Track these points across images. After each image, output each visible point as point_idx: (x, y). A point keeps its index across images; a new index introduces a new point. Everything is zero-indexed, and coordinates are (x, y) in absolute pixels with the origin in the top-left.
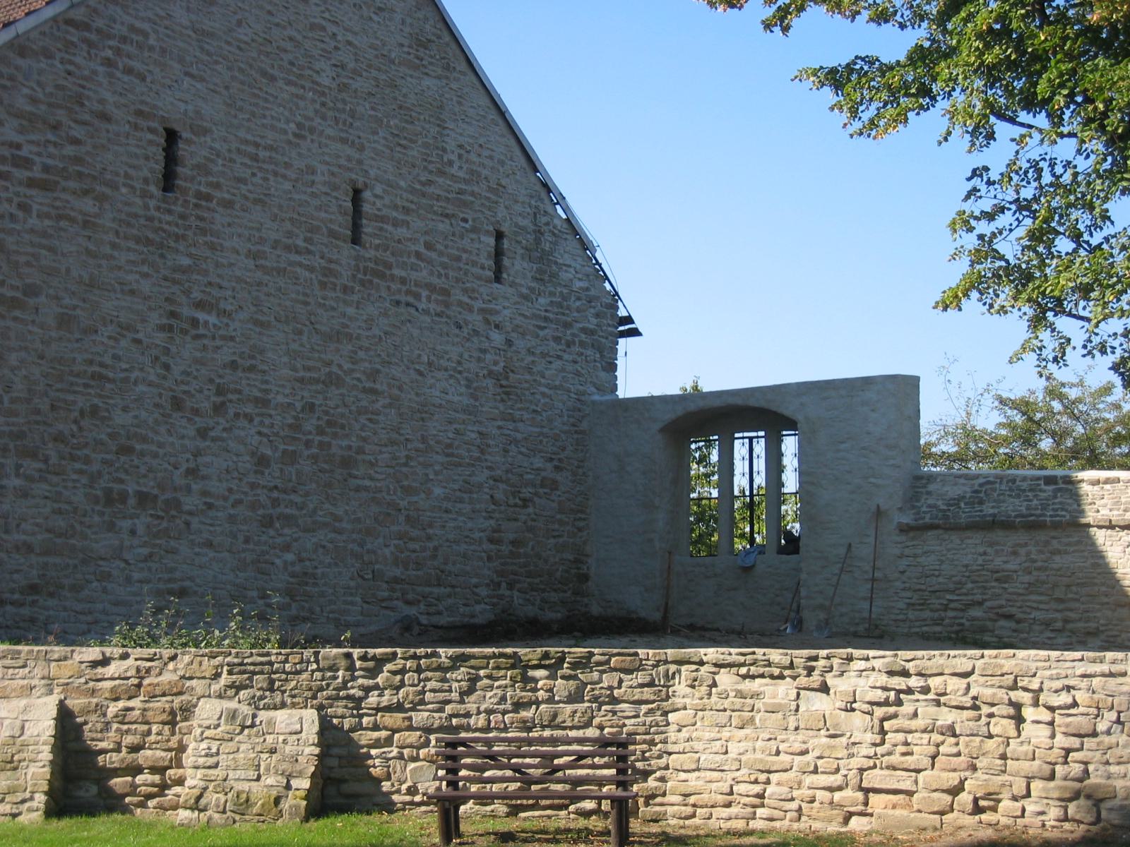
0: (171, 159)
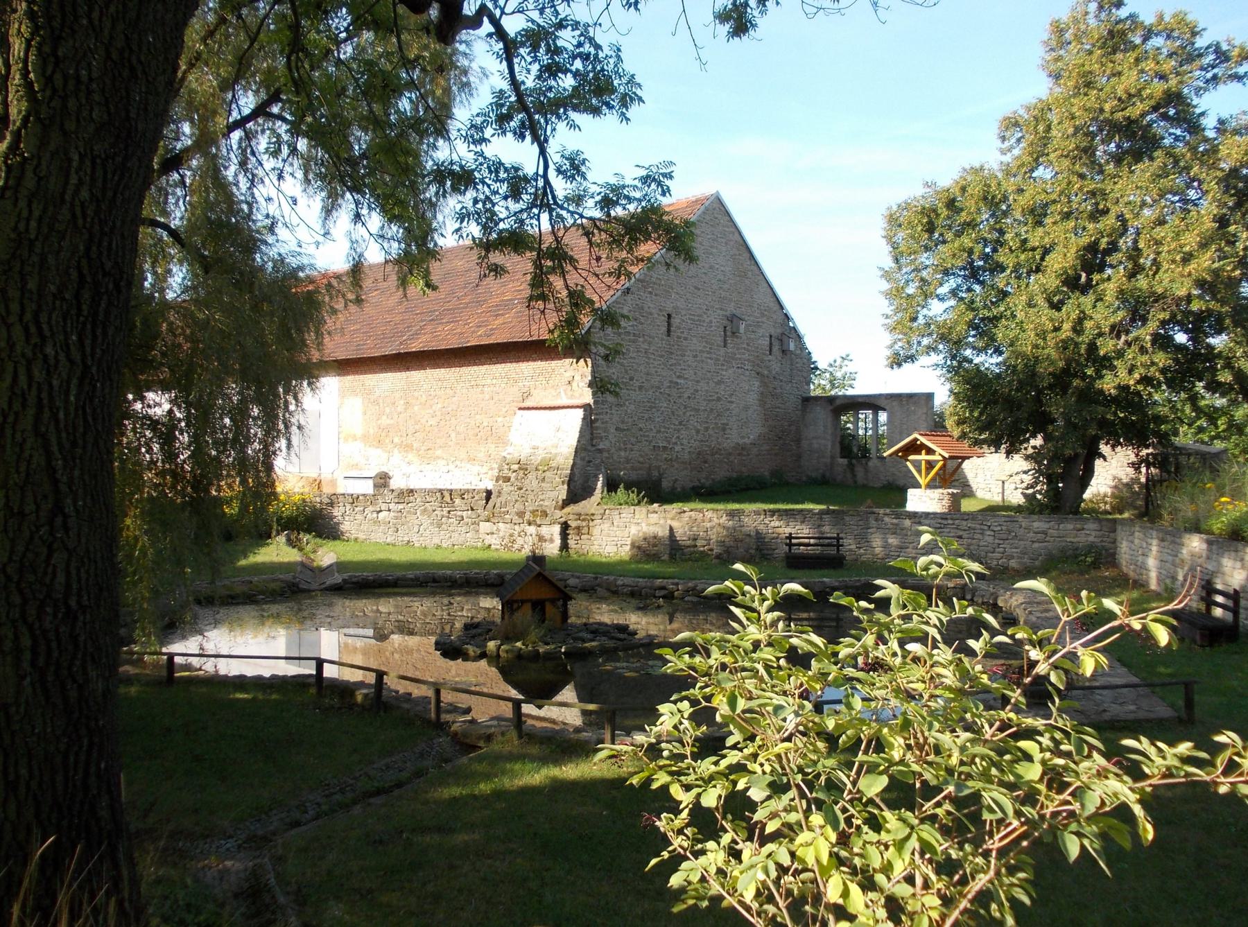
0: (669, 325)
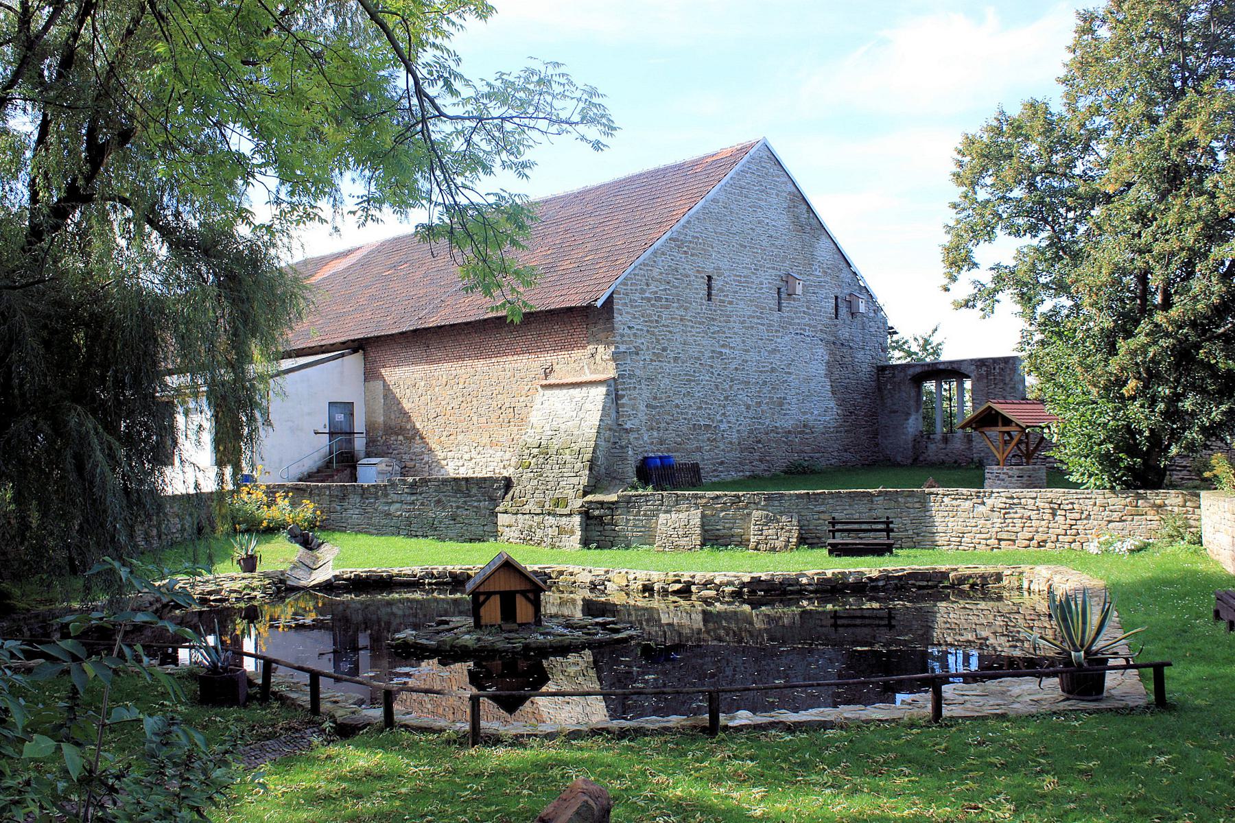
0: (710, 287)
